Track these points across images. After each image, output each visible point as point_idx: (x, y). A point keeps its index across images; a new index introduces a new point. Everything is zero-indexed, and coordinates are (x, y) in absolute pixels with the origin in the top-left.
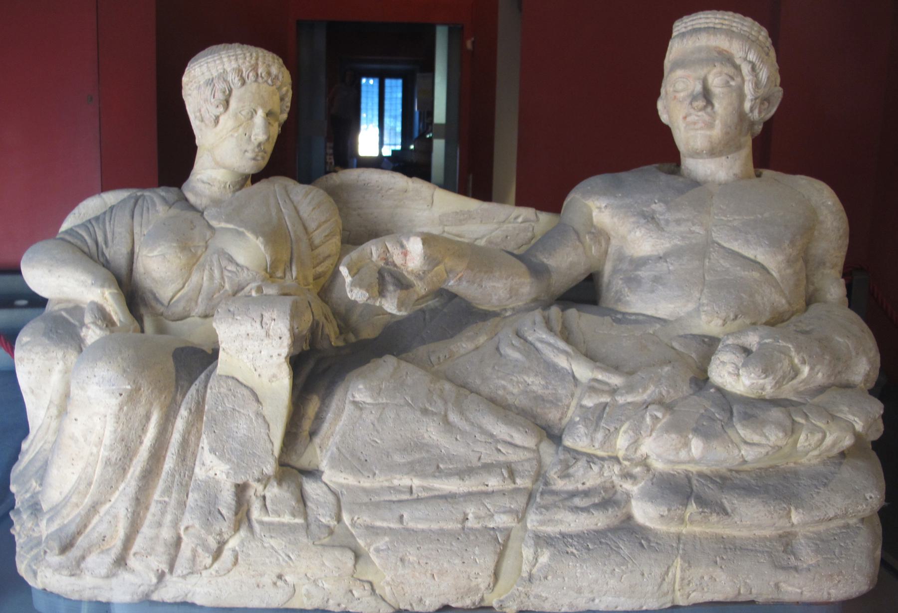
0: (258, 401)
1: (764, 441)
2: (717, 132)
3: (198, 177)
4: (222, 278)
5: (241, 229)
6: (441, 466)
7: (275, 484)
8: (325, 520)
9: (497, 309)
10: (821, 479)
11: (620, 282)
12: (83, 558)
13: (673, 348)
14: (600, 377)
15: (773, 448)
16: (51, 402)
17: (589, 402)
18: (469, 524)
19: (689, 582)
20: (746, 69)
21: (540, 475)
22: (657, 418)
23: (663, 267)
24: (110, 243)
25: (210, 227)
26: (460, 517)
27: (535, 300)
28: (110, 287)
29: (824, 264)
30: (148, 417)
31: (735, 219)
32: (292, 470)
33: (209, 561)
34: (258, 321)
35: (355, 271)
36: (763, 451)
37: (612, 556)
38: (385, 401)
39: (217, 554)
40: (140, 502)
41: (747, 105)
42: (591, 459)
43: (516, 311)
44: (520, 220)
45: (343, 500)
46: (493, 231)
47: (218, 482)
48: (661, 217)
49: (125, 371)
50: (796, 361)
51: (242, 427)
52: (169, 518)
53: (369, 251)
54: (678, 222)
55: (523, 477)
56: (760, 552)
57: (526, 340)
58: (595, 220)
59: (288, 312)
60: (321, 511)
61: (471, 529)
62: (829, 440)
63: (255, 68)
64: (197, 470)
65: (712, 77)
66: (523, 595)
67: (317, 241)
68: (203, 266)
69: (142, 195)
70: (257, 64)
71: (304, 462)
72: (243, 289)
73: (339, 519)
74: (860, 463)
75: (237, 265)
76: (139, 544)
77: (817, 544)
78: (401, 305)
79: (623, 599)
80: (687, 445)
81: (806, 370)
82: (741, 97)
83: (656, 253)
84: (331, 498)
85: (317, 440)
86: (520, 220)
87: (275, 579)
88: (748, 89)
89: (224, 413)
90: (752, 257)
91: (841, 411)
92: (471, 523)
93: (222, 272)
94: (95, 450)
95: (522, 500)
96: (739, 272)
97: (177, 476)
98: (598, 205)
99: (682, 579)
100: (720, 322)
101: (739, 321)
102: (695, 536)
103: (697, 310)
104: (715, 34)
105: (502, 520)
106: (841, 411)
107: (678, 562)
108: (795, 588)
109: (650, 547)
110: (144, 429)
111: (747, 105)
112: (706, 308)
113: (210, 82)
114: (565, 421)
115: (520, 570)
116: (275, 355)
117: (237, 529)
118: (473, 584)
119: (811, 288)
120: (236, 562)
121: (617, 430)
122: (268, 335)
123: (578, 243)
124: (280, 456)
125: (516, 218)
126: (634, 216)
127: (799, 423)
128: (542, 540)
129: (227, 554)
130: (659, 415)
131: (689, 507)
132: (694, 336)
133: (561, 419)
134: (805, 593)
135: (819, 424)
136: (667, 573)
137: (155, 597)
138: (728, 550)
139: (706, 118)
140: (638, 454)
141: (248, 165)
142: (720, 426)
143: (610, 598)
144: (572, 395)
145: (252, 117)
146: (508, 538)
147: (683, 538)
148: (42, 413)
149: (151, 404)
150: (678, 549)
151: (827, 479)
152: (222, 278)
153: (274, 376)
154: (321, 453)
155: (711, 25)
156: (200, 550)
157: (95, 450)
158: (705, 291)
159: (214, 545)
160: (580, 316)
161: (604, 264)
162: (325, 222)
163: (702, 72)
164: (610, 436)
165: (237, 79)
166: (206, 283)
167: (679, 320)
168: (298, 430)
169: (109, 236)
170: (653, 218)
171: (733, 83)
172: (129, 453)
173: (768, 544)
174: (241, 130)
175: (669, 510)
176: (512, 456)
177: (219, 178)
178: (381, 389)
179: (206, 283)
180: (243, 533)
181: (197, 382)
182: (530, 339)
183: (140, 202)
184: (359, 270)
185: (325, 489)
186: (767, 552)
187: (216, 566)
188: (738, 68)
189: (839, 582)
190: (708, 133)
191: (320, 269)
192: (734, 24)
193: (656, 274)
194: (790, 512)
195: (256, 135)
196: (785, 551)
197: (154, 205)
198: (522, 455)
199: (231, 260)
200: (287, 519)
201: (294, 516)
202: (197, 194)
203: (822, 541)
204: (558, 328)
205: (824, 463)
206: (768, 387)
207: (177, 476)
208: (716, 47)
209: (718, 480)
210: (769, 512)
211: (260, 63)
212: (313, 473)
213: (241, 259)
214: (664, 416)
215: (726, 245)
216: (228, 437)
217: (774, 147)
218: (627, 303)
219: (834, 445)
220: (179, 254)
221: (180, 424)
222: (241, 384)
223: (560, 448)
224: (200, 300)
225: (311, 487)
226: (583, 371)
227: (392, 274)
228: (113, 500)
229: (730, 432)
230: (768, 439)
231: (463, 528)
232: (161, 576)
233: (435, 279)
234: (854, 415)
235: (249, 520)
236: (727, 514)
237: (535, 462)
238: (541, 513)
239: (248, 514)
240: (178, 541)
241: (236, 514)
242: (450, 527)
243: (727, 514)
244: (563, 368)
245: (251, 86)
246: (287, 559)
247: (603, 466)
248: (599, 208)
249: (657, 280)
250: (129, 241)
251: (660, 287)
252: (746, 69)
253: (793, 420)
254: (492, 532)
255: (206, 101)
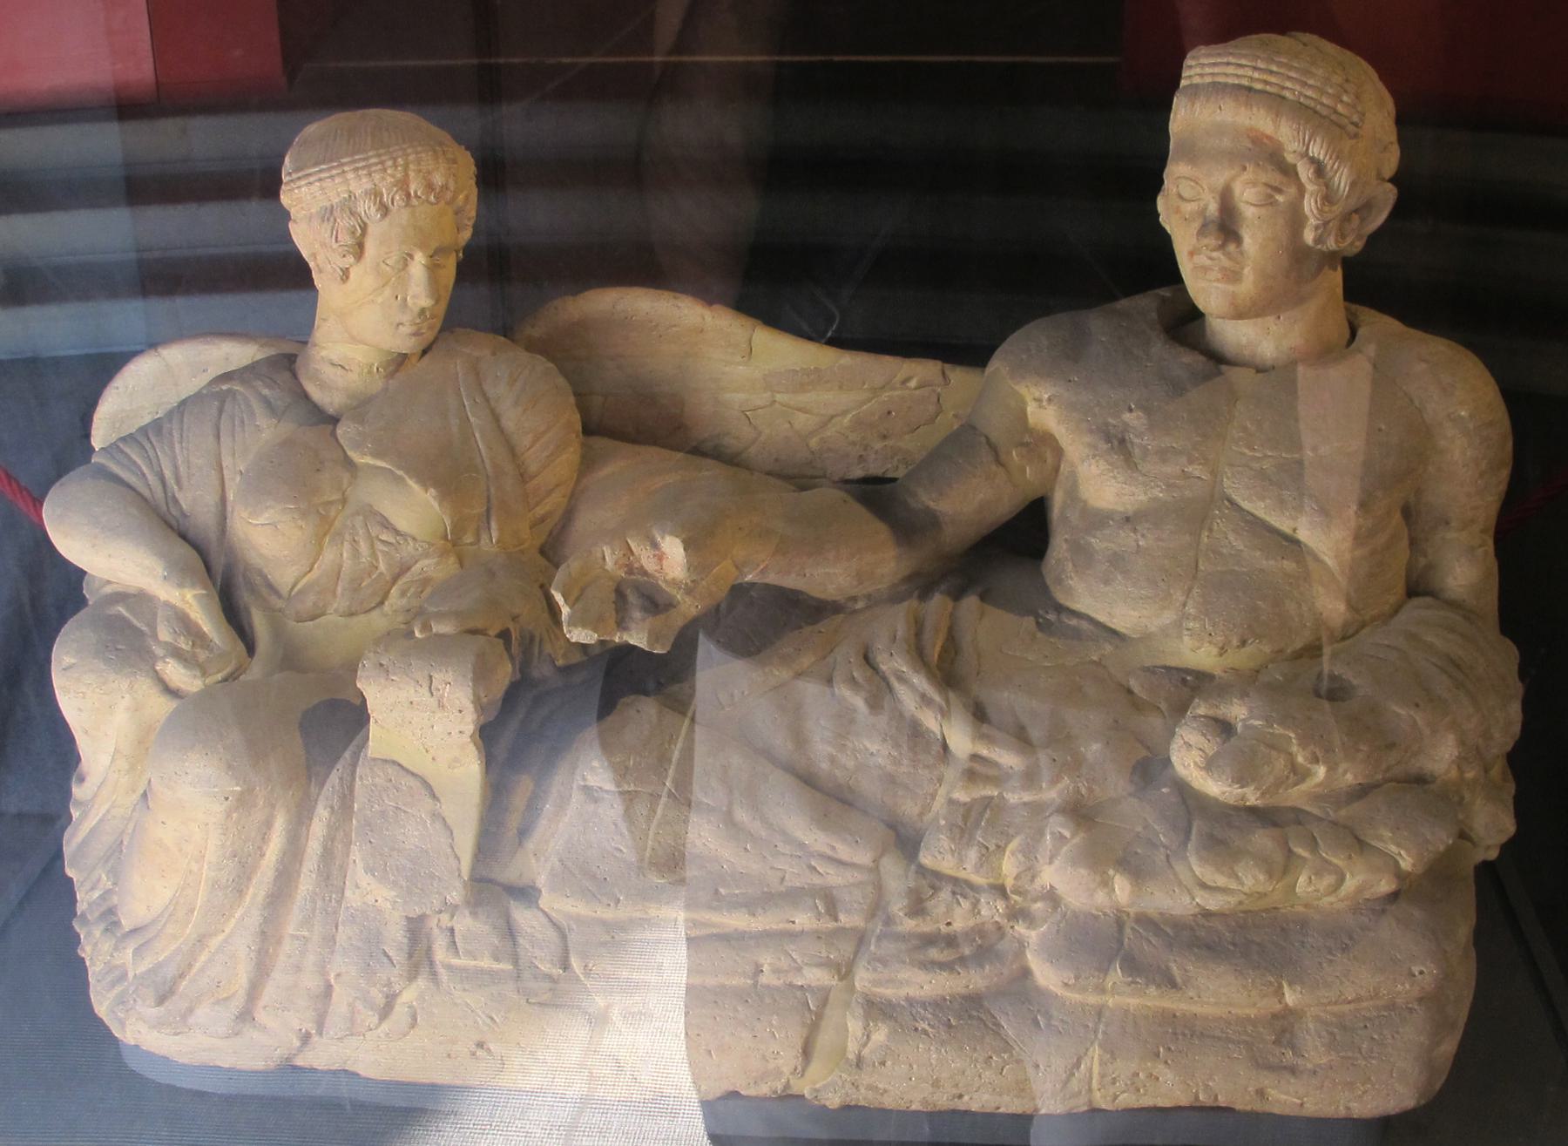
0: (434, 796)
1: (1233, 885)
2: (1248, 285)
3: (324, 353)
4: (374, 554)
5: (400, 473)
6: (722, 890)
7: (467, 912)
8: (545, 967)
9: (839, 598)
10: (1341, 937)
11: (1065, 546)
12: (191, 1010)
13: (1130, 692)
14: (984, 752)
15: (1248, 895)
16: (116, 751)
17: (961, 796)
18: (764, 979)
19: (1114, 1081)
20: (1305, 172)
21: (877, 908)
22: (1062, 837)
23: (1127, 539)
24: (185, 482)
25: (349, 464)
26: (749, 969)
27: (909, 579)
28: (193, 586)
29: (1447, 523)
30: (268, 824)
31: (1266, 456)
32: (494, 889)
33: (376, 1020)
34: (426, 685)
35: (575, 593)
36: (1233, 900)
37: (987, 1040)
38: (632, 788)
39: (386, 1011)
40: (268, 936)
41: (1309, 236)
42: (961, 887)
43: (873, 601)
44: (913, 384)
45: (573, 938)
46: (863, 403)
47: (380, 911)
48: (1137, 441)
49: (230, 767)
50: (1300, 759)
51: (413, 833)
52: (311, 959)
53: (599, 555)
54: (1164, 455)
55: (848, 912)
56: (1233, 1042)
57: (875, 669)
58: (1031, 420)
59: (470, 675)
60: (537, 953)
61: (768, 987)
62: (1350, 884)
63: (403, 184)
64: (348, 893)
65: (1258, 158)
66: (848, 1086)
67: (533, 468)
68: (340, 534)
69: (229, 391)
70: (407, 175)
71: (511, 873)
72: (409, 569)
73: (566, 966)
74: (1417, 913)
75: (397, 532)
76: (269, 993)
77: (1331, 1033)
78: (655, 637)
79: (1006, 1098)
80: (1106, 883)
81: (1321, 771)
82: (1296, 220)
84: (551, 934)
85: (530, 845)
86: (913, 384)
87: (473, 1048)
88: (1309, 205)
89: (383, 814)
90: (1288, 531)
91: (1380, 838)
92: (767, 978)
93: (372, 546)
94: (194, 867)
95: (847, 948)
96: (1258, 559)
97: (319, 903)
98: (1037, 394)
99: (1102, 1076)
100: (1215, 651)
101: (1248, 649)
102: (1127, 1011)
103: (1178, 625)
104: (1248, 105)
105: (815, 976)
106: (1380, 838)
107: (1096, 1051)
108: (1286, 1097)
109: (1049, 1025)
110: (265, 839)
111: (1309, 236)
113: (328, 214)
114: (928, 817)
115: (844, 1049)
116: (455, 733)
117: (412, 976)
118: (771, 1066)
119: (1422, 561)
120: (414, 1023)
121: (1001, 849)
122: (441, 706)
123: (994, 467)
124: (473, 869)
125: (904, 382)
126: (1091, 431)
127: (1300, 857)
128: (877, 1009)
129: (400, 1010)
130: (1067, 834)
131: (1111, 972)
132: (1168, 669)
133: (921, 815)
134: (1307, 1105)
135: (1335, 861)
136: (1077, 1065)
137: (299, 1062)
138: (1177, 1035)
139: (1226, 262)
140: (1038, 882)
141: (403, 341)
142: (1163, 857)
143: (986, 1097)
144: (940, 780)
145: (406, 265)
146: (824, 1002)
147: (1107, 1014)
148: (105, 760)
149: (273, 806)
150: (1096, 1032)
151: (1351, 938)
152: (374, 554)
153: (456, 760)
154: (537, 862)
155: (1245, 82)
156: (359, 1006)
157: (194, 867)
158: (1196, 590)
159: (380, 1000)
160: (982, 614)
161: (1052, 489)
162: (545, 432)
163: (1220, 177)
164: (988, 857)
165: (373, 209)
166: (347, 564)
167: (1147, 637)
168: (499, 824)
169: (182, 470)
170: (1122, 441)
171: (1280, 198)
172: (245, 871)
173: (1250, 1029)
174: (388, 292)
175: (1077, 978)
176: (834, 877)
177: (359, 358)
178: (627, 768)
179: (347, 564)
180: (421, 983)
181: (339, 766)
182: (883, 667)
183: (228, 406)
184: (583, 590)
185: (544, 920)
186: (1245, 1042)
187: (385, 1026)
188: (1289, 171)
189: (1365, 1092)
190: (1231, 288)
191: (540, 511)
192: (1288, 84)
194: (1280, 987)
195: (414, 297)
196: (1277, 1042)
197: (252, 414)
198: (852, 876)
199: (386, 524)
200: (486, 963)
201: (497, 960)
202: (323, 386)
203: (1344, 1028)
204: (934, 653)
205: (1356, 910)
206: (1252, 797)
207: (319, 903)
208: (1251, 129)
209: (1169, 930)
210: (1244, 987)
211: (412, 174)
212: (526, 893)
213: (402, 524)
214: (1073, 836)
215: (1246, 505)
216: (393, 849)
217: (1391, 278)
218: (1069, 591)
219: (1360, 890)
220: (300, 522)
222: (407, 771)
223: (913, 867)
224: (339, 589)
225: (523, 917)
226: (961, 740)
227: (637, 588)
228: (227, 931)
229: (1179, 867)
230: (1242, 884)
231: (755, 984)
232: (306, 1038)
233: (714, 589)
234: (1398, 845)
235: (431, 963)
236: (1173, 985)
237: (870, 889)
238: (875, 970)
239: (429, 951)
240: (328, 990)
241: (410, 956)
242: (1251, 278)
243: (1173, 985)
244: (928, 730)
245: (400, 215)
246: (488, 1021)
247: (978, 901)
248: (1039, 400)
249: (1117, 561)
250: (217, 483)
252: (1305, 172)
253: (1290, 851)
254: (799, 993)
255: (323, 245)
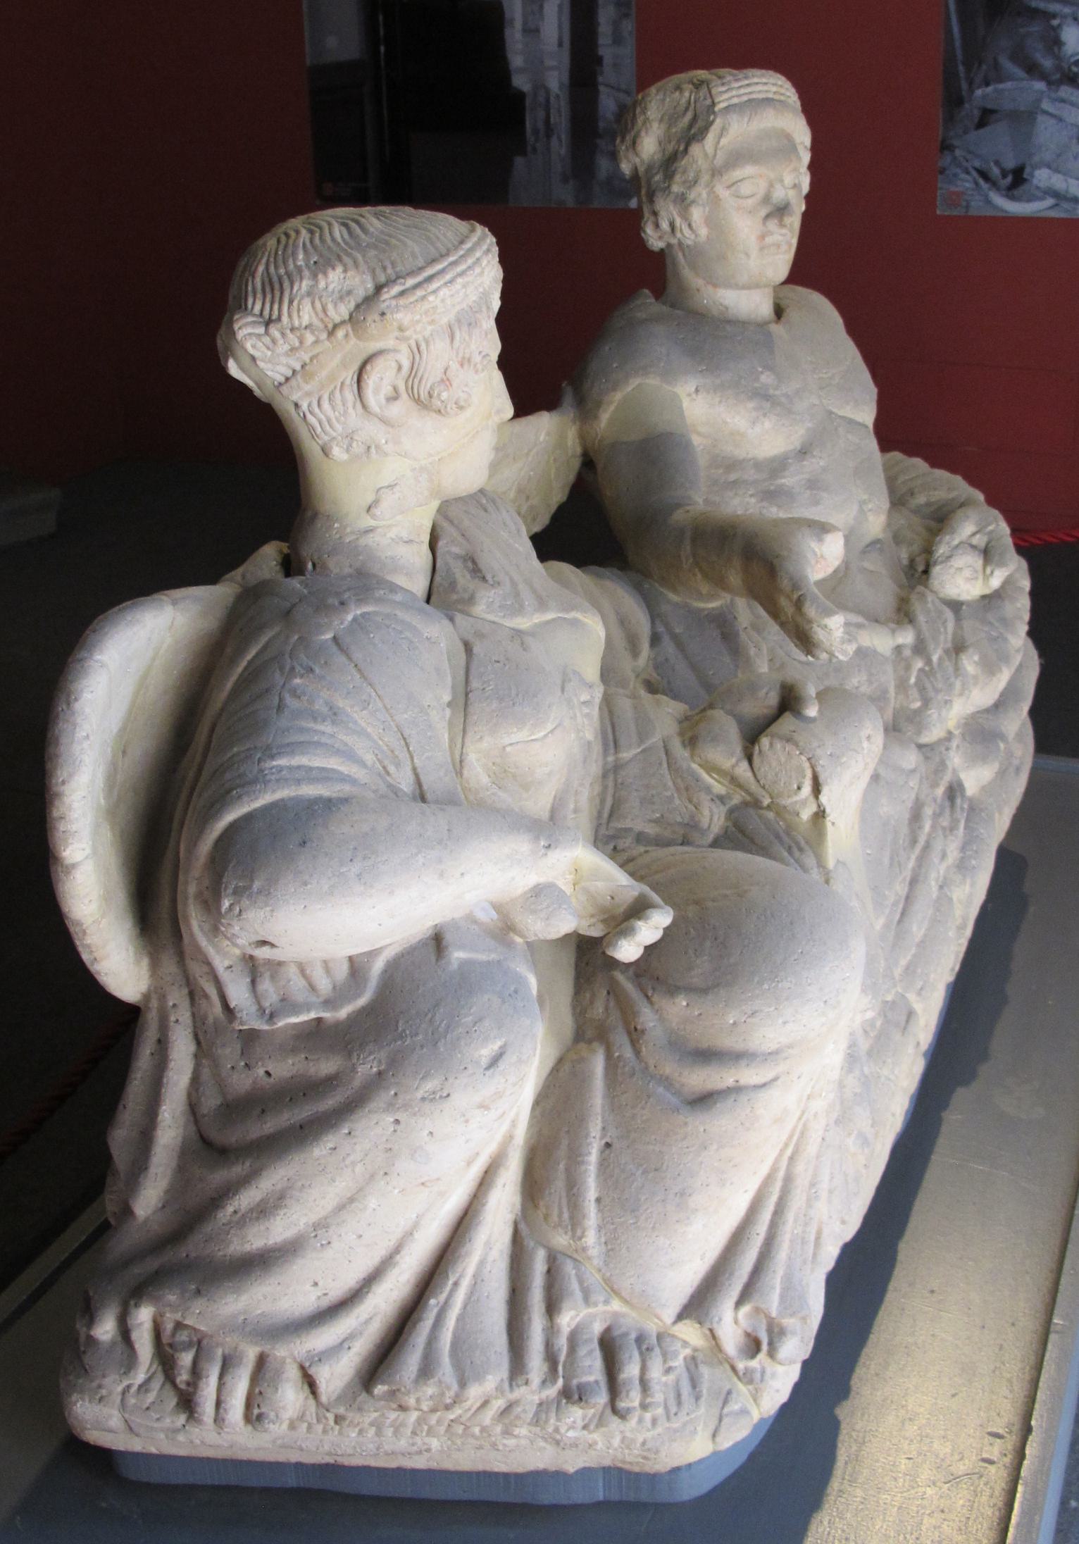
23: (814, 464)
48: (777, 393)
83: (792, 447)
112: (870, 506)
193: (806, 476)
221: (271, 1125)
251: (825, 495)
